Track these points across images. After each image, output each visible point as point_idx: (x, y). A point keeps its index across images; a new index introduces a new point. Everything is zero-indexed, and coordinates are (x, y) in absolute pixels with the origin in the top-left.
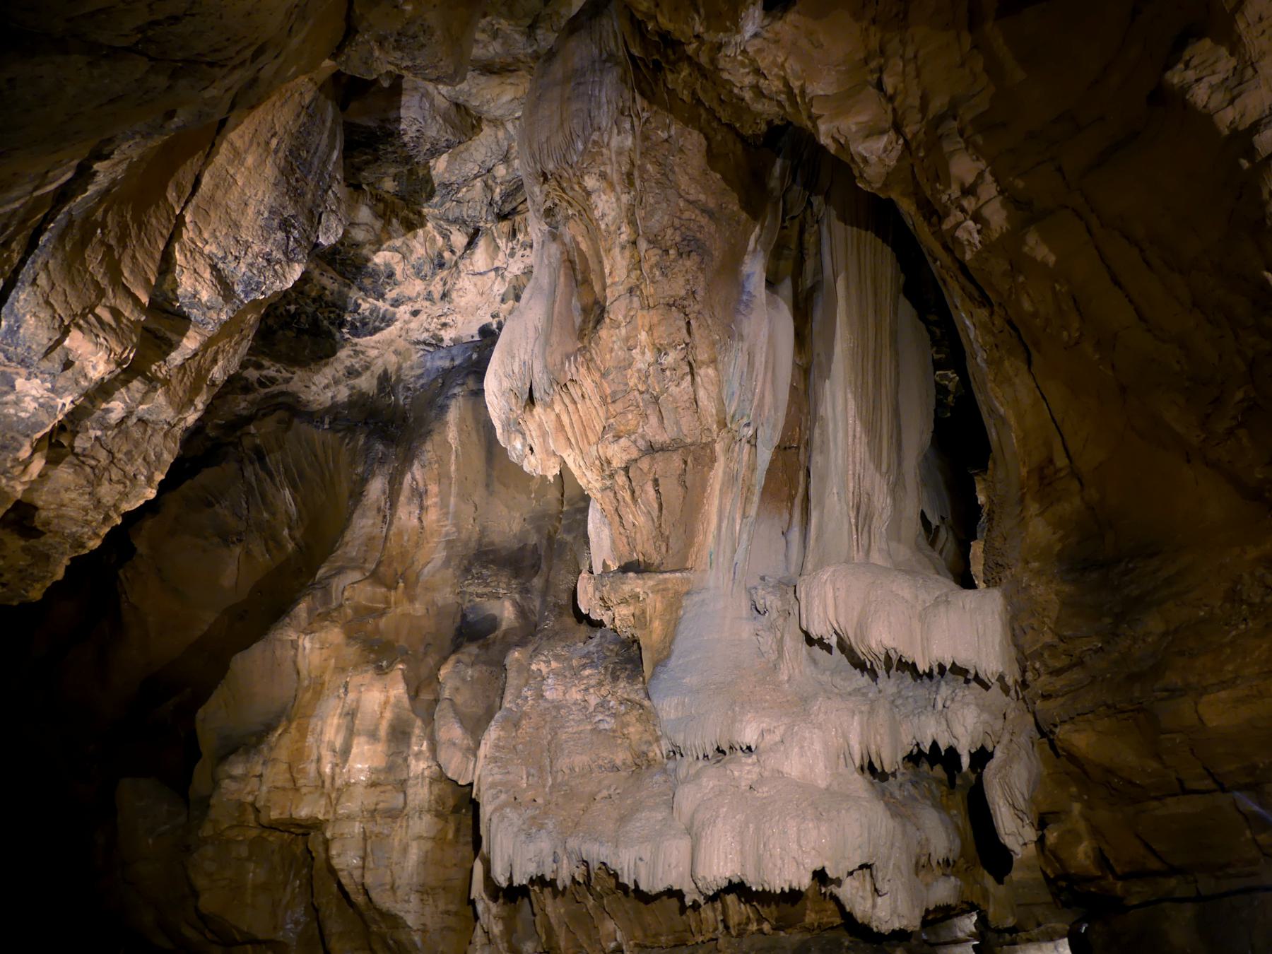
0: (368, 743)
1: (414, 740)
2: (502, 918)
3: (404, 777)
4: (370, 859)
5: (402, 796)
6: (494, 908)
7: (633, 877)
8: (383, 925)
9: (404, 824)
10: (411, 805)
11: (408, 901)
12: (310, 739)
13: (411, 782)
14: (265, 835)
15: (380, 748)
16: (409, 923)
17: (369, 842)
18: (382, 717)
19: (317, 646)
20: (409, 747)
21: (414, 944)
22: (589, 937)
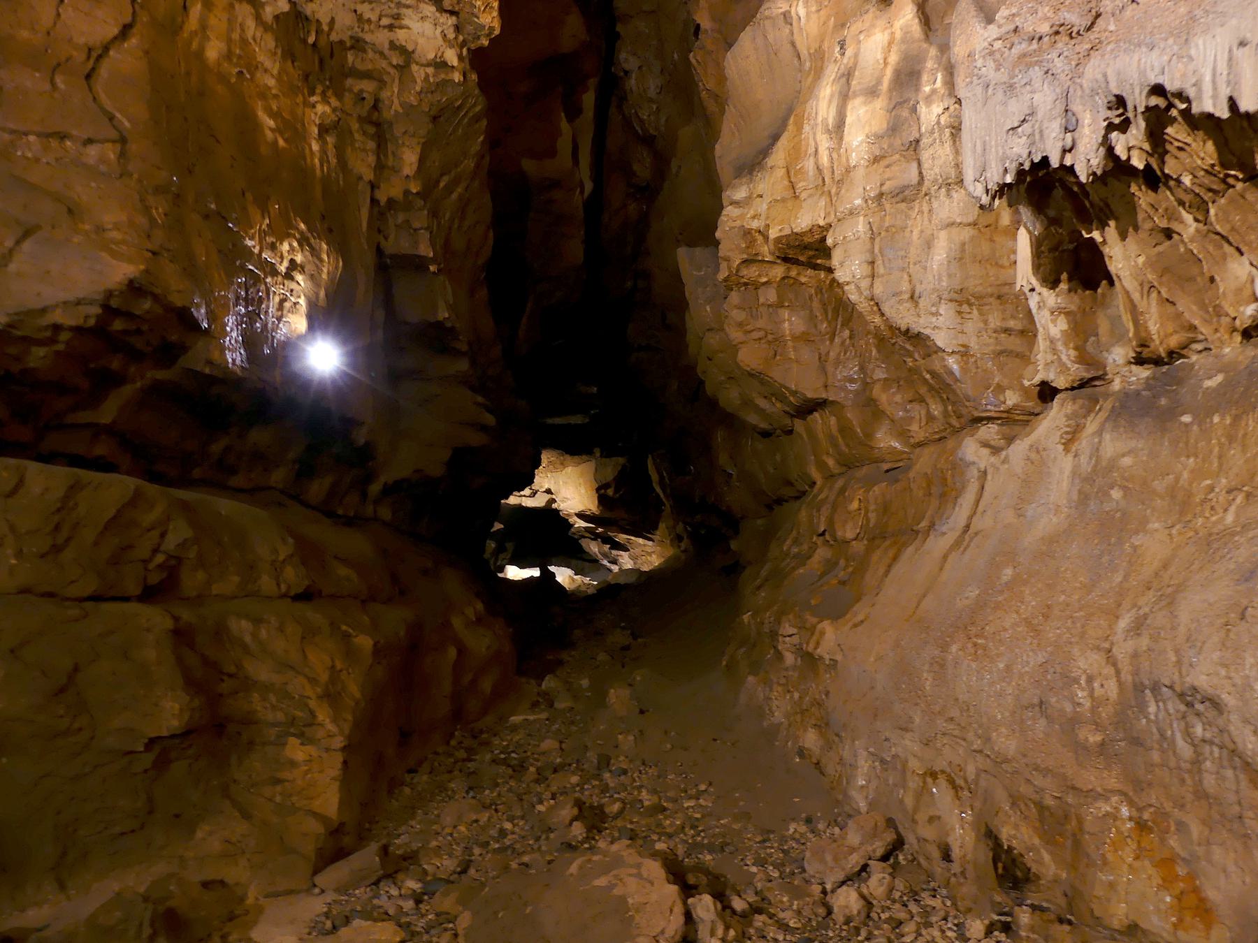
0: (865, 103)
1: (925, 77)
2: (1068, 314)
3: (916, 135)
4: (879, 262)
5: (915, 165)
6: (1050, 298)
7: (1225, 92)
8: (916, 356)
9: (925, 208)
10: (929, 175)
11: (937, 314)
12: (807, 128)
13: (925, 141)
14: (793, 273)
15: (880, 104)
16: (940, 344)
17: (877, 240)
18: (886, 63)
19: (814, 9)
20: (917, 89)
21: (951, 373)
22: (1203, 306)
